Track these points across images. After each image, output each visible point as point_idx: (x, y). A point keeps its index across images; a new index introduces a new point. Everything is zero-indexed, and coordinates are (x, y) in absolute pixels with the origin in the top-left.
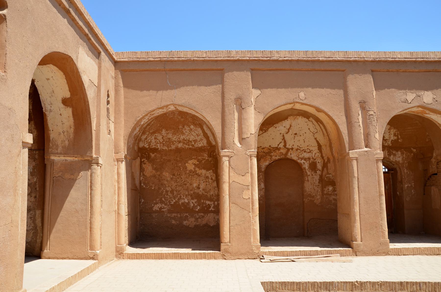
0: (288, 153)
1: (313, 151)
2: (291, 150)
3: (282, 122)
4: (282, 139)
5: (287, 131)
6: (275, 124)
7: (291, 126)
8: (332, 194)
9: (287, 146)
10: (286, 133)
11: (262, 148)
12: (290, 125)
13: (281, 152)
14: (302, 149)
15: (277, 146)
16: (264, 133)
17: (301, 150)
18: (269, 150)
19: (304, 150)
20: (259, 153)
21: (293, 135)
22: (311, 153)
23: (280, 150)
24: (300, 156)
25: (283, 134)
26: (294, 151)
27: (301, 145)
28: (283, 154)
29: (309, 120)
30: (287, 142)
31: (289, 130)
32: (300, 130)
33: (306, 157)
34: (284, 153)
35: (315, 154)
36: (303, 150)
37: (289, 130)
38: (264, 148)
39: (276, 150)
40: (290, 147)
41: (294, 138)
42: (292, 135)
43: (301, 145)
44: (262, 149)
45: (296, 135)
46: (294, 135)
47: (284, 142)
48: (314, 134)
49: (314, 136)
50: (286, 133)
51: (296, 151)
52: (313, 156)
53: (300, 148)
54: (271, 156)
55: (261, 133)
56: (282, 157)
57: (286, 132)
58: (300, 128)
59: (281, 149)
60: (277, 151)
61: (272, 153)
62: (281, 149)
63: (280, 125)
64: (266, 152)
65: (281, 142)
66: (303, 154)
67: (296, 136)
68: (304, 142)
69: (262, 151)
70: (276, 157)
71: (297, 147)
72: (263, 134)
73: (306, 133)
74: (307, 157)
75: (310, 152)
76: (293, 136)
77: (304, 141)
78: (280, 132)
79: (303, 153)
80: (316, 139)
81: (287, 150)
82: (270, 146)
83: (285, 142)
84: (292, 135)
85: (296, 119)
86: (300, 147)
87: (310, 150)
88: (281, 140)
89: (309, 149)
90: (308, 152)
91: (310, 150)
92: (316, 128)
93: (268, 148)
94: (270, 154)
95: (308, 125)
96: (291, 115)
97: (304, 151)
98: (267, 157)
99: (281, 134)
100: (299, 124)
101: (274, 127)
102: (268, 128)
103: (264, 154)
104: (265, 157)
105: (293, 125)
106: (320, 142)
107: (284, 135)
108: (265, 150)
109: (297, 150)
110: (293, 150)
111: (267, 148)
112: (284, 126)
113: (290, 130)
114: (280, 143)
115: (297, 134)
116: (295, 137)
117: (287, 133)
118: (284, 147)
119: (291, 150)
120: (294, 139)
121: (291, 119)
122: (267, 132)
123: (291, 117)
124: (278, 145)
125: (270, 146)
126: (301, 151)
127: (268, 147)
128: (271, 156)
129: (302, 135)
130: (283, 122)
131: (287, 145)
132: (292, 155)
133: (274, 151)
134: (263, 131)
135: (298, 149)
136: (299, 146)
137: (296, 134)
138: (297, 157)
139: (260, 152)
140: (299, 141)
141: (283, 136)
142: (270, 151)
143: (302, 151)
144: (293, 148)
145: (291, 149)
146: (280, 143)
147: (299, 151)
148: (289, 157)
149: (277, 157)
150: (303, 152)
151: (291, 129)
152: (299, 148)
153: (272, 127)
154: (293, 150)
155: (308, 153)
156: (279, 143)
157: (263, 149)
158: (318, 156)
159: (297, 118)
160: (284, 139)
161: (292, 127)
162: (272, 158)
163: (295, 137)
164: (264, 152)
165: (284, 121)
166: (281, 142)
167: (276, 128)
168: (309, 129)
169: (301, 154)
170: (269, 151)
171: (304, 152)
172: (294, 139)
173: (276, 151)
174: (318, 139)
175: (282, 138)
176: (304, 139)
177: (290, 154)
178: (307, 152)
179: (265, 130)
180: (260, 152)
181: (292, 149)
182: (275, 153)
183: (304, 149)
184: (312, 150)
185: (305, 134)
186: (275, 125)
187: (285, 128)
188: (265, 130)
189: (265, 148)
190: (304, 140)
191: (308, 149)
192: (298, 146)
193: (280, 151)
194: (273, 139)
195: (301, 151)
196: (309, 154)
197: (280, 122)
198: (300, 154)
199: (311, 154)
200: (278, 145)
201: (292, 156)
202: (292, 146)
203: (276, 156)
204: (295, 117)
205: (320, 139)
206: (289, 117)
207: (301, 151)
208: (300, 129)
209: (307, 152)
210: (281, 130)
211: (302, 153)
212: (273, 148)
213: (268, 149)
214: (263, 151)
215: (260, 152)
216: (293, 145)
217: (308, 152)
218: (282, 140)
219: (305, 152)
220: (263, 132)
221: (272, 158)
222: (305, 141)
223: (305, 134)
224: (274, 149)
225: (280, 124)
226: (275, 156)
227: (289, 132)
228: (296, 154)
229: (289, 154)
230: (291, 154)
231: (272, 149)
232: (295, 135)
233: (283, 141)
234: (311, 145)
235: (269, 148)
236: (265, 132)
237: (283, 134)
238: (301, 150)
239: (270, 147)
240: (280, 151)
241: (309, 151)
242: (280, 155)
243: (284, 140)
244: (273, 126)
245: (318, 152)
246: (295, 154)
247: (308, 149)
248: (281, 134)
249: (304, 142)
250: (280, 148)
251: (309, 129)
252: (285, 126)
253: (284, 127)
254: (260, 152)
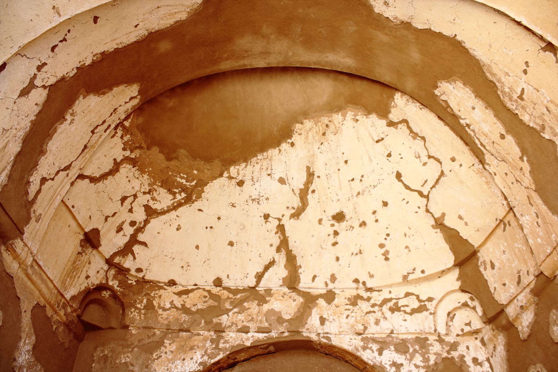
0: (310, 314)
1: (434, 303)
2: (321, 302)
3: (265, 154)
4: (274, 248)
5: (296, 202)
6: (233, 162)
7: (310, 175)
8: (109, 293)
9: (305, 283)
10: (293, 216)
11: (180, 288)
12: (308, 168)
13: (271, 312)
14: (377, 298)
15: (252, 282)
16: (180, 205)
17: (372, 301)
18: (211, 302)
19: (390, 300)
20: (160, 312)
21: (327, 222)
22: (425, 313)
23: (266, 302)
24: (373, 330)
25: (279, 220)
26: (337, 307)
27: (372, 276)
28: (280, 320)
29: (391, 124)
30: (299, 262)
31: (303, 194)
32: (359, 193)
33: (404, 337)
34: (287, 317)
35: (451, 315)
36: (385, 301)
37: (303, 194)
38: (187, 292)
39: (245, 300)
40: (318, 288)
41: (332, 240)
42: (320, 221)
43: (372, 276)
44: (176, 297)
45: (344, 224)
46: (333, 225)
47: (287, 260)
48: (427, 197)
49: (427, 211)
50: (293, 216)
51: (351, 307)
52: (442, 330)
53: (368, 294)
54: (219, 330)
55: (170, 203)
56: (274, 334)
57: (293, 211)
58: (357, 181)
59: (271, 295)
60: (253, 307)
61: (227, 311)
62: (271, 295)
63: (261, 169)
64: (194, 309)
65: (272, 263)
66: (385, 318)
67: (340, 227)
68: (387, 259)
69: (178, 302)
70: (244, 335)
71: (354, 285)
72: (181, 209)
73: (385, 204)
74: (410, 337)
75: (421, 309)
76: (327, 228)
77: (383, 251)
78: (265, 208)
79: (388, 314)
80: (439, 224)
81: (301, 300)
82: (218, 282)
83: (291, 260)
84: (320, 221)
85: (330, 136)
86: (369, 285)
87: (420, 301)
88: (271, 253)
89: (412, 294)
90: (414, 311)
91: (420, 301)
92: (430, 157)
93: (209, 292)
94: (215, 320)
95: (389, 155)
96: (305, 114)
97: (391, 304)
98: (199, 335)
99: (266, 217)
100: (346, 162)
101: (234, 182)
102: (202, 184)
103: (184, 317)
104: (188, 331)
105: (318, 170)
106: (464, 234)
107: (283, 225)
108: (190, 301)
109: (354, 301)
110: (334, 299)
111: (204, 290)
112: (277, 176)
113: (310, 197)
114: (267, 268)
115: (347, 217)
116: (336, 233)
117: (296, 215)
118: (289, 288)
119: (321, 302)
120: (335, 244)
121: (307, 138)
122: (197, 205)
123: (308, 124)
124: (259, 277)
125: (218, 282)
126: (373, 306)
127: (208, 288)
128: (219, 330)
129: (370, 219)
130: (273, 152)
131: (302, 277)
132: (327, 322)
133: (239, 304)
134: (174, 194)
135: (362, 298)
136: (364, 283)
137: (339, 217)
138: (360, 334)
139: (168, 306)
140: (360, 252)
141: (281, 228)
142: (216, 304)
143: (381, 306)
144: (334, 294)
145: (321, 296)
146: (267, 268)
147: (364, 306)
148: (314, 337)
149: (247, 332)
150: (385, 308)
151: (313, 191)
152: (365, 295)
153: (223, 180)
154: (336, 301)
155: (411, 314)
156: (260, 270)
157: (184, 296)
158: (469, 324)
159: (332, 126)
160: (284, 244)
161: (316, 180)
162: (222, 337)
163: (336, 233)
164: (185, 310)
165: (276, 151)
166: (272, 263)
167: (241, 183)
168: (399, 176)
169: (377, 322)
170: (210, 307)
171: (392, 310)
172: (335, 244)
173: (246, 304)
174: (450, 222)
175: (276, 241)
176: (384, 242)
177: (318, 322)
178: (408, 310)
179: (184, 189)
180: (164, 310)
181: (330, 297)
182: (239, 313)
183: (389, 296)
184: (430, 299)
185: (382, 212)
186: (233, 170)
187: (285, 188)
188: (183, 190)
189: (192, 290)
190: (382, 246)
191: (408, 295)
192: (356, 281)
193: (266, 307)
194: (231, 244)
195: (373, 306)
196: (418, 316)
197: (260, 157)
198: (371, 318)
199: (427, 318)
200: (259, 277)
201: (331, 328)
202: (327, 284)
203: (245, 330)
204: (325, 120)
205: (462, 214)
206: (298, 126)
207: (376, 309)
208: (357, 186)
209: (405, 312)
210: (267, 199)
211: (380, 313)
212: (235, 292)
213: (206, 294)
214: (183, 305)
215: (168, 306)
216: (333, 278)
217: (414, 311)
218: (278, 250)
219: (395, 309)
220: (179, 197)
221: (222, 337)
222: (387, 252)
223: (382, 212)
224: (238, 296)
225: (257, 167)
226: (239, 331)
227: (308, 208)
228: (351, 320)
229: (314, 320)
230: (323, 321)
231: (228, 298)
232: (336, 224)
233: (281, 259)
234: (423, 272)
235: (215, 290)
236: (188, 200)
237: (279, 220)
238: (372, 301)
239: (219, 288)
240: (266, 307)
241: (416, 304)
242: (267, 325)
243: (283, 252)
244: (226, 174)
245: (465, 305)
246: (344, 320)
247: (408, 295)
248: (266, 217)
249: (387, 259)
250: (269, 292)
251: (399, 176)
252: (284, 176)
253: (282, 181)
254: (164, 310)
